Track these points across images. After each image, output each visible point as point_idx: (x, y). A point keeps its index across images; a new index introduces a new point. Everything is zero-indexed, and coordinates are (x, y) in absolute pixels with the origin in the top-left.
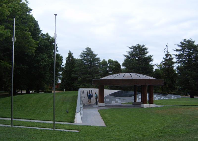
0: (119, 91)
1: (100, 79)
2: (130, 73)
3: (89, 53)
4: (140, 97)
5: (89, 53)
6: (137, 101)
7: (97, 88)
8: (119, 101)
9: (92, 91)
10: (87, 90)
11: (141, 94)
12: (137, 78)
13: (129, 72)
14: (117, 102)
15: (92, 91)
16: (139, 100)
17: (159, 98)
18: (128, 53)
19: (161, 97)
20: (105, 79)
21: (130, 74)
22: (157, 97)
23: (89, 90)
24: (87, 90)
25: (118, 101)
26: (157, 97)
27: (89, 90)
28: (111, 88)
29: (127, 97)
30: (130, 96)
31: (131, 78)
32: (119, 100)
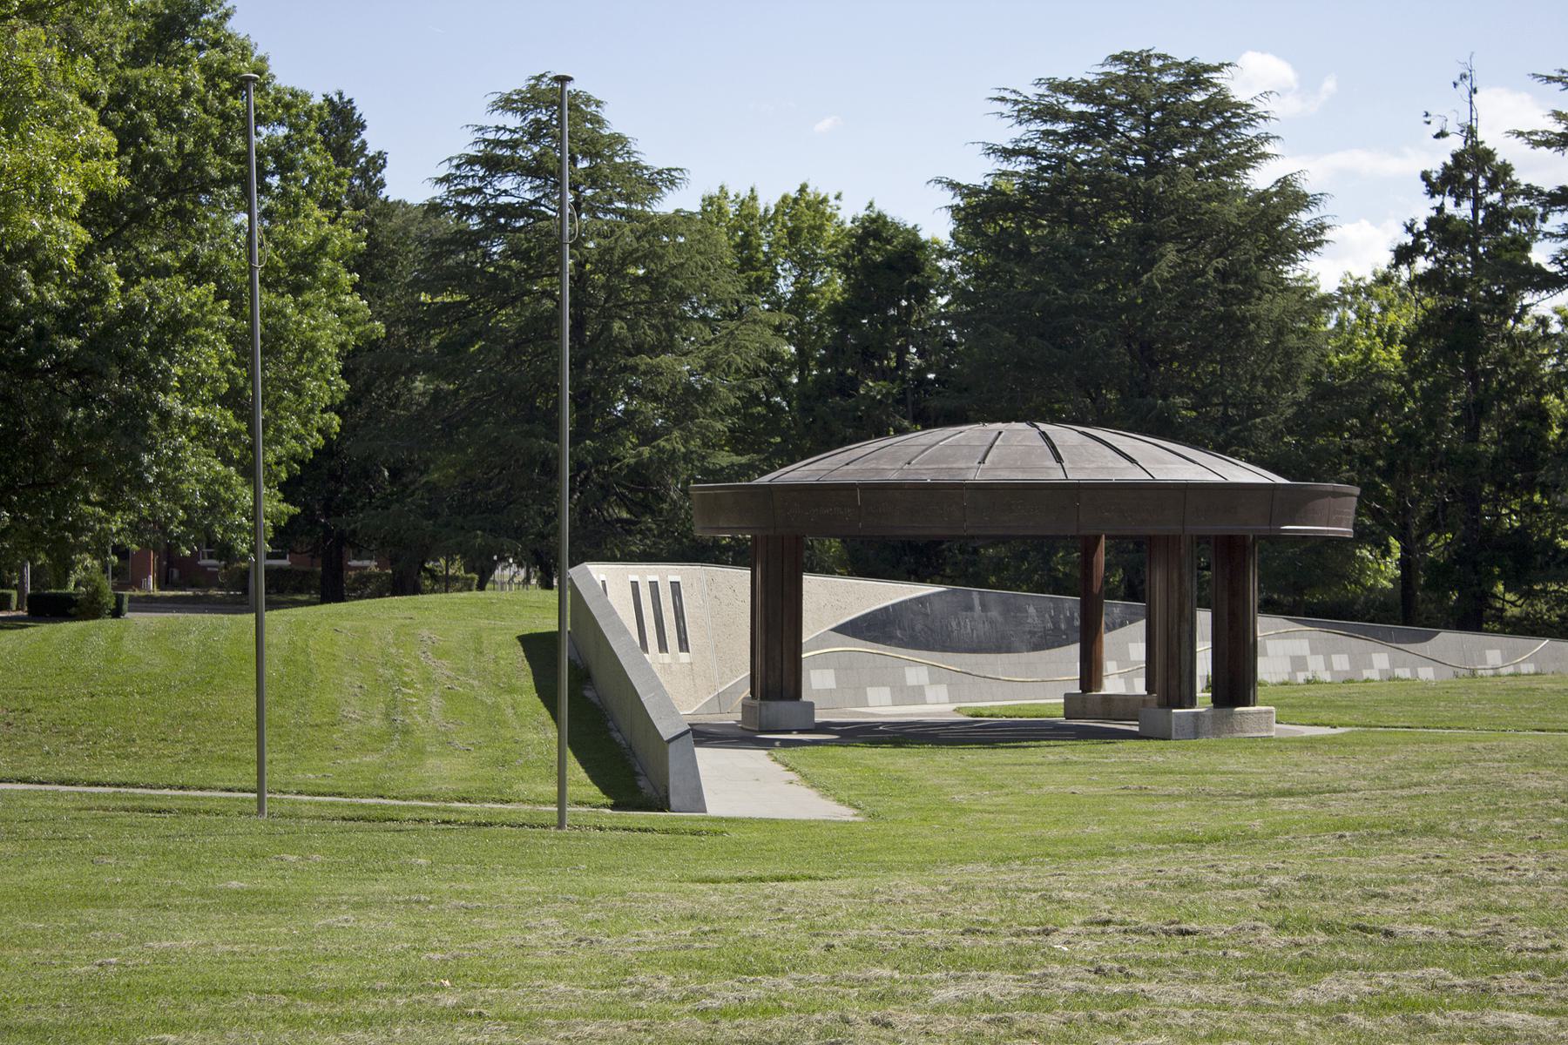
0: (934, 594)
1: (765, 480)
2: (1043, 427)
3: (555, 128)
4: (1138, 651)
5: (555, 128)
6: (1112, 685)
7: (736, 563)
8: (928, 688)
9: (675, 586)
10: (635, 585)
11: (1141, 625)
12: (1114, 477)
13: (1030, 417)
14: (917, 695)
15: (675, 586)
16: (1125, 665)
17: (1341, 663)
18: (999, 107)
19: (1359, 662)
20: (812, 480)
21: (1044, 435)
22: (1314, 651)
23: (654, 586)
24: (635, 585)
25: (921, 688)
26: (1314, 651)
27: (654, 586)
28: (863, 564)
29: (1060, 646)
30: (1046, 641)
31: (1056, 475)
32: (933, 682)
